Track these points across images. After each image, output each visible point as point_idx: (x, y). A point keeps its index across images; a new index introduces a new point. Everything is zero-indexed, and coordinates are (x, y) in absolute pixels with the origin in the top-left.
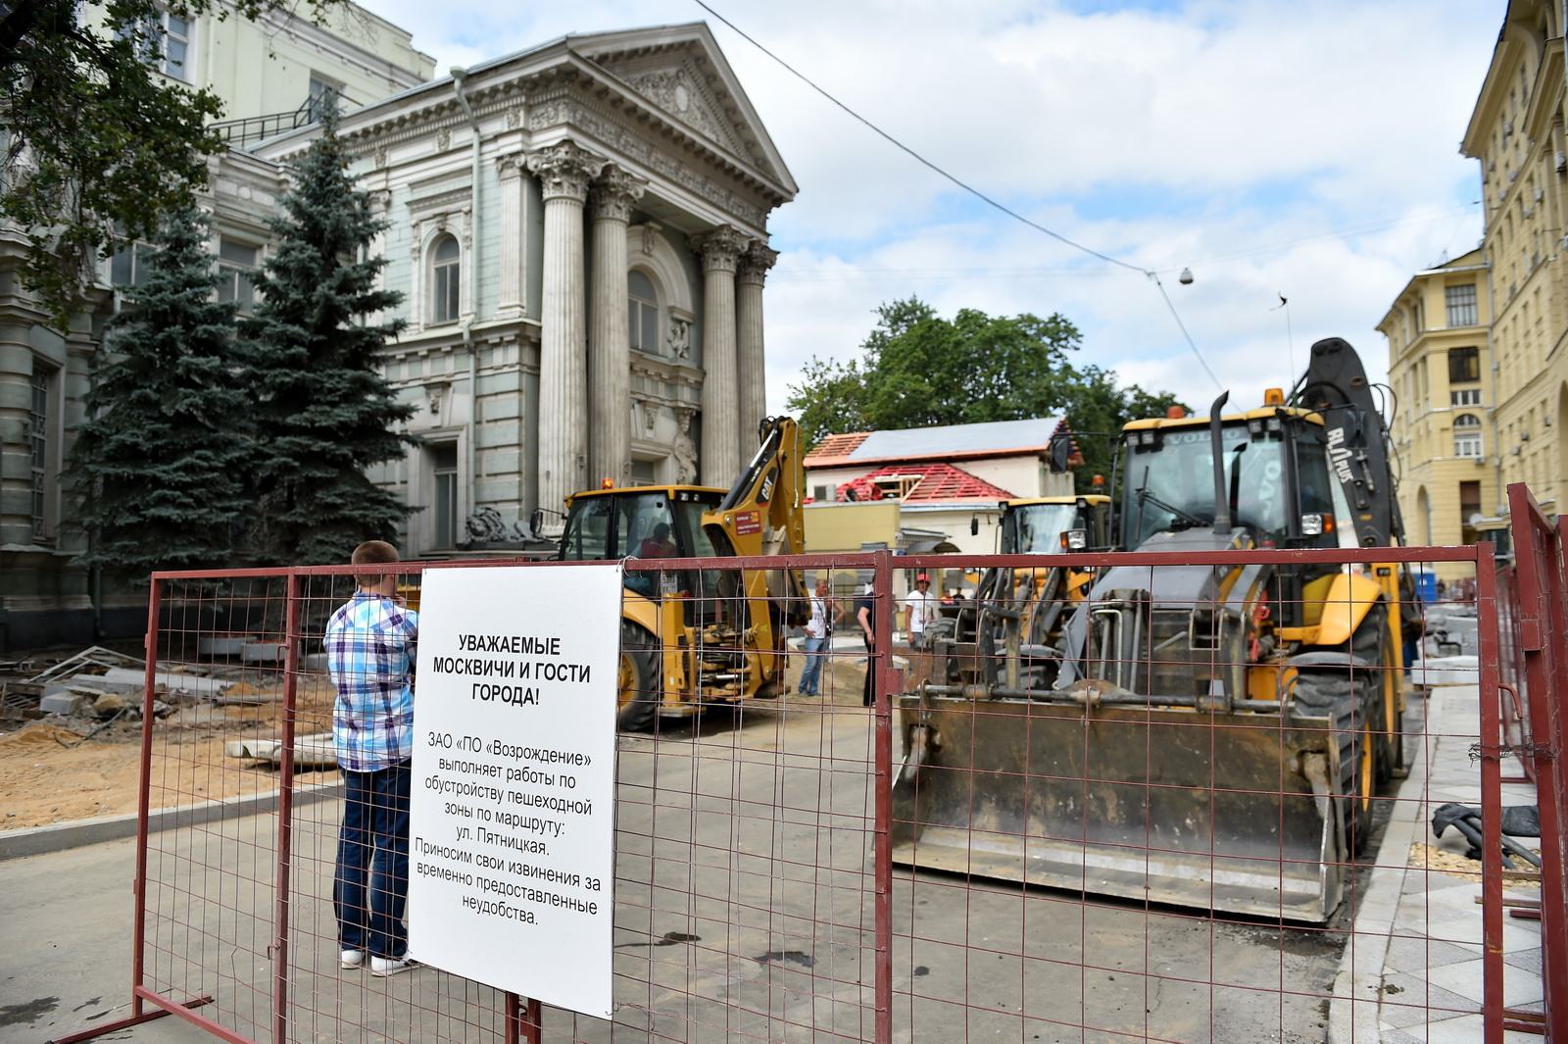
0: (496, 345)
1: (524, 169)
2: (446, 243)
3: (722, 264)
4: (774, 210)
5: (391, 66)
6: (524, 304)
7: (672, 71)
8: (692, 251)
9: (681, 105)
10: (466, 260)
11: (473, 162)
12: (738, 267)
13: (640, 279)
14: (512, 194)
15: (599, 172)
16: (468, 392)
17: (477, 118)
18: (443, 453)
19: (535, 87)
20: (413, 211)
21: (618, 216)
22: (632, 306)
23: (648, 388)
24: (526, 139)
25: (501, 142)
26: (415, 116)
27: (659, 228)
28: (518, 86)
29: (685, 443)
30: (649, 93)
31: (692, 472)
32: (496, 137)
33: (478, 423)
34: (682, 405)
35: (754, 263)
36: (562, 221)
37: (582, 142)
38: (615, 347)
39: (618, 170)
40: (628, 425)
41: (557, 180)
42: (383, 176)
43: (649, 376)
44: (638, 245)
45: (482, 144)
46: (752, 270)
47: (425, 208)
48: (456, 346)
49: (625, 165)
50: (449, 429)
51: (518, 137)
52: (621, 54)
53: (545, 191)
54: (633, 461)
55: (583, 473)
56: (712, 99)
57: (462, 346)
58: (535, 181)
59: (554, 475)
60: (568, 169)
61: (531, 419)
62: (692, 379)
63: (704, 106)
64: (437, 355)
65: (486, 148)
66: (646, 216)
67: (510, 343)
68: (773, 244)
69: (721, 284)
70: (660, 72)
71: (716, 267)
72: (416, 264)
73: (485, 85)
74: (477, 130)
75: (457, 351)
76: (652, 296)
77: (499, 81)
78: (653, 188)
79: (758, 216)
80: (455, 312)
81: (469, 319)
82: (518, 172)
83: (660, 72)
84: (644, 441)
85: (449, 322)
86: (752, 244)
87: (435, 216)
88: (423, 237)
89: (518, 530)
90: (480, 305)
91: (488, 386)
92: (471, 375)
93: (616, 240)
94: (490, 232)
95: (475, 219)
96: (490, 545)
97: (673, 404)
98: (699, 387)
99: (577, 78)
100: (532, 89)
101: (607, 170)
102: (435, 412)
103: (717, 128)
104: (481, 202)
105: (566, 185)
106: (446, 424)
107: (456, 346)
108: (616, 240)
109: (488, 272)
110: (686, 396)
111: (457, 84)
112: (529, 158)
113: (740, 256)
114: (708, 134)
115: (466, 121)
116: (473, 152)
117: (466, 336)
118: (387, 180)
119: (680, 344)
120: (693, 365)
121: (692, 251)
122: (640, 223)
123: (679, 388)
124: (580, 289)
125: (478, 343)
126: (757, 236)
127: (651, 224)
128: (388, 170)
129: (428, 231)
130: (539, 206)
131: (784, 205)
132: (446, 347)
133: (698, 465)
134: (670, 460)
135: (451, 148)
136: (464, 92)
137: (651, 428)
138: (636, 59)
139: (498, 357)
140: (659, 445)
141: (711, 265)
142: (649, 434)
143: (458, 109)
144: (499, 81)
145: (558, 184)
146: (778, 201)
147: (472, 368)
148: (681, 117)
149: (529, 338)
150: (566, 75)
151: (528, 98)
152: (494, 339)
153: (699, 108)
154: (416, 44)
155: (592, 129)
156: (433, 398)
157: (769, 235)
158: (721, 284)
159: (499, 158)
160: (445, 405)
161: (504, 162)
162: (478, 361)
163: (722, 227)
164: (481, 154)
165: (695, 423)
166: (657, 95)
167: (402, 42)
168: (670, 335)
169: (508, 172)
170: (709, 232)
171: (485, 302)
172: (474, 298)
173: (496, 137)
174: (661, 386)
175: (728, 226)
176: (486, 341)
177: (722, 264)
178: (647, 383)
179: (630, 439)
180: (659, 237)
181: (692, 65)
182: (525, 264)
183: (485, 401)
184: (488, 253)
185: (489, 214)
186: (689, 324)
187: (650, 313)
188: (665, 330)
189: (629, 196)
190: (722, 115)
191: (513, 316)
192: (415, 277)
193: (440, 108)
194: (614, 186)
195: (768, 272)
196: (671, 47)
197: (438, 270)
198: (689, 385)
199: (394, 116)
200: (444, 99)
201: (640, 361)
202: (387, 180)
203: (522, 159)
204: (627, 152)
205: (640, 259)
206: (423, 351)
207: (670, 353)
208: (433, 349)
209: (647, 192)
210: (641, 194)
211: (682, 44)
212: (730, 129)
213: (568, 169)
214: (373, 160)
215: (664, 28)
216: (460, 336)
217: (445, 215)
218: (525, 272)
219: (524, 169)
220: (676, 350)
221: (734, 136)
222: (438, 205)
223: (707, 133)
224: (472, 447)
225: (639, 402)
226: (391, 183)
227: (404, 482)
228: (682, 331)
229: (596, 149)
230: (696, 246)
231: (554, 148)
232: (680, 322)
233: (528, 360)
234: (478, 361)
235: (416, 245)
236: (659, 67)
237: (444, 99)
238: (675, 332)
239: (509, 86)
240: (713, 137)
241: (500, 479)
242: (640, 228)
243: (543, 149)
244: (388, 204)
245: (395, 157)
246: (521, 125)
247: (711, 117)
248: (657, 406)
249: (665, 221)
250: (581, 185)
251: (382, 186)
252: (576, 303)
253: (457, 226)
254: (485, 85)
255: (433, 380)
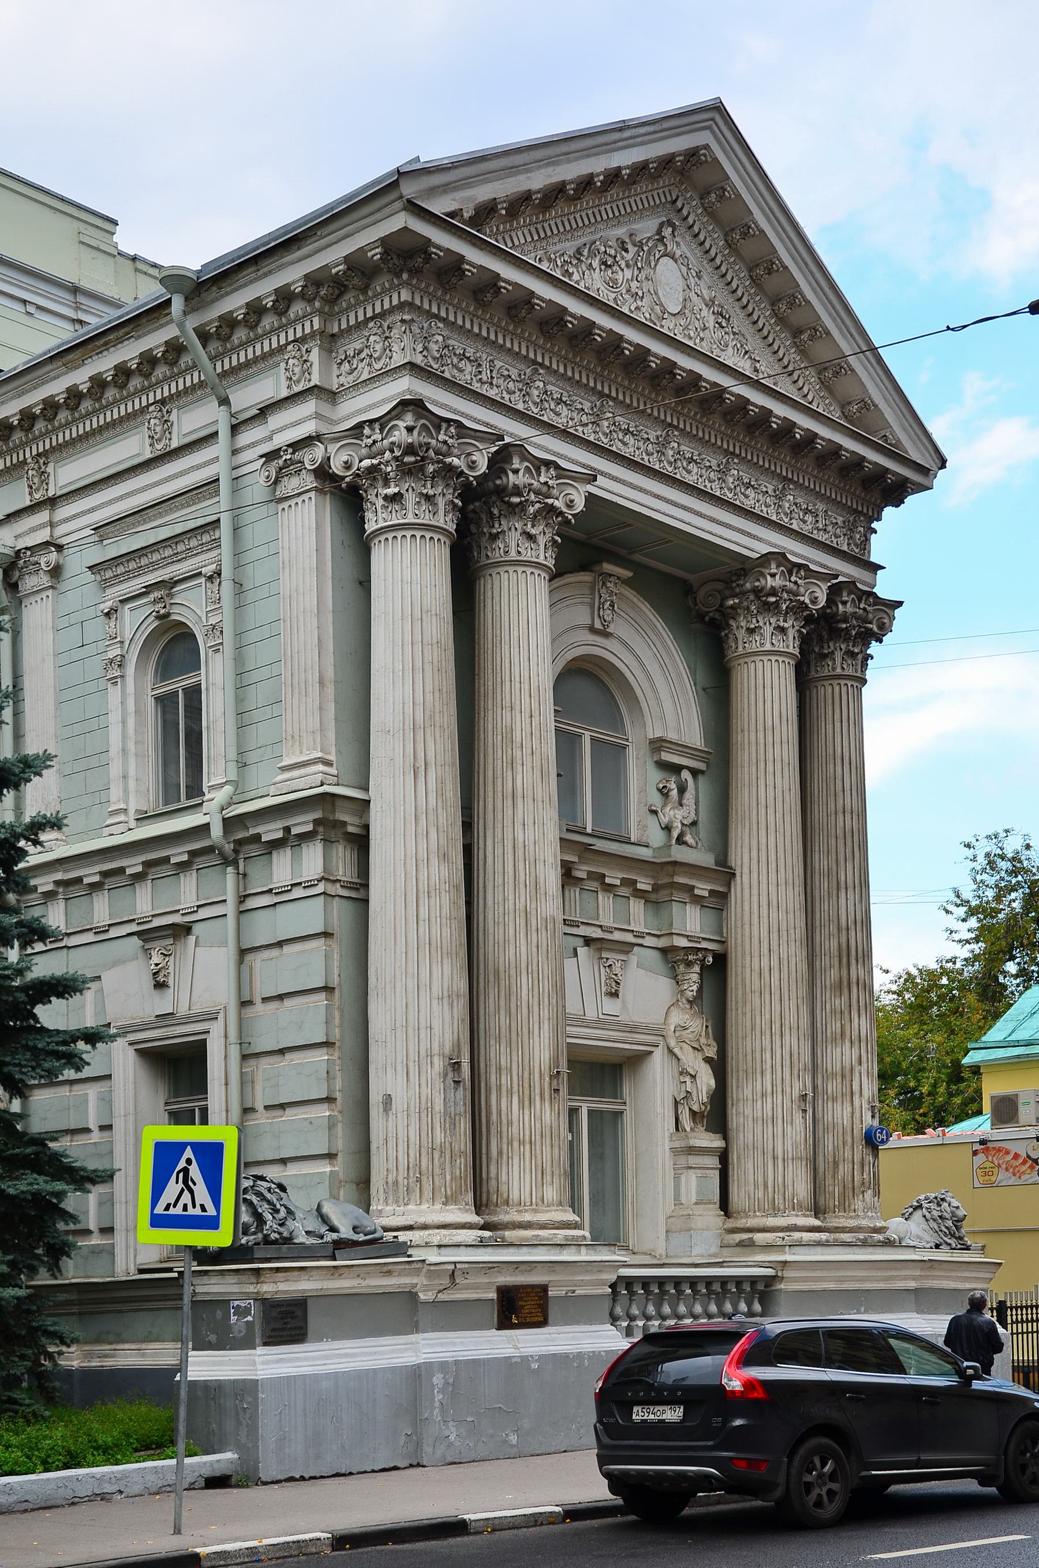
0: (276, 845)
1: (323, 473)
2: (174, 647)
3: (767, 639)
4: (888, 512)
5: (75, 290)
6: (332, 757)
7: (646, 227)
8: (701, 617)
9: (666, 294)
10: (215, 675)
11: (222, 469)
12: (805, 642)
13: (588, 685)
14: (304, 528)
15: (483, 467)
16: (225, 944)
17: (224, 374)
18: (180, 1067)
19: (331, 290)
20: (105, 585)
21: (528, 555)
22: (567, 744)
23: (606, 910)
24: (325, 409)
25: (275, 420)
26: (98, 384)
27: (627, 574)
28: (302, 296)
29: (697, 1026)
30: (595, 282)
31: (707, 1080)
32: (264, 412)
33: (245, 1004)
34: (683, 943)
35: (842, 630)
36: (411, 575)
37: (442, 401)
38: (529, 831)
39: (525, 456)
40: (560, 989)
41: (392, 490)
42: (43, 516)
43: (609, 888)
44: (582, 615)
45: (235, 429)
46: (838, 649)
47: (129, 575)
48: (198, 852)
49: (544, 446)
50: (189, 1020)
51: (309, 407)
52: (526, 197)
53: (369, 515)
54: (571, 1063)
55: (462, 1095)
56: (740, 278)
57: (210, 850)
58: (348, 496)
59: (398, 1104)
60: (413, 463)
61: (354, 991)
62: (703, 888)
63: (723, 298)
64: (164, 871)
65: (245, 438)
66: (596, 548)
67: (305, 837)
68: (884, 588)
69: (767, 684)
70: (621, 232)
71: (497, 556)
72: (114, 694)
73: (234, 302)
74: (224, 401)
75: (200, 862)
76: (616, 722)
77: (262, 288)
78: (606, 489)
79: (850, 528)
80: (195, 789)
81: (220, 796)
82: (310, 481)
83: (621, 232)
84: (599, 1024)
85: (185, 803)
86: (835, 591)
87: (149, 589)
88: (128, 636)
89: (324, 1219)
90: (242, 766)
91: (264, 928)
92: (230, 909)
93: (528, 616)
94: (258, 613)
95: (227, 587)
96: (270, 1251)
97: (662, 943)
98: (719, 902)
99: (413, 254)
100: (332, 301)
101: (500, 461)
102: (160, 986)
103: (754, 343)
104: (237, 554)
105: (410, 499)
106: (183, 1010)
107: (198, 852)
108: (528, 616)
109: (257, 696)
110: (691, 922)
111: (178, 304)
112: (332, 448)
113: (809, 620)
114: (734, 355)
115: (202, 384)
116: (219, 449)
117: (217, 831)
118: (52, 525)
119: (676, 816)
120: (705, 858)
121: (701, 617)
122: (584, 567)
123: (676, 907)
124: (448, 717)
125: (242, 842)
126: (847, 570)
127: (608, 567)
128: (52, 502)
129: (136, 622)
130: (360, 546)
131: (909, 500)
132: (178, 854)
133: (720, 1067)
134: (658, 1056)
135: (175, 444)
136: (192, 323)
137: (615, 995)
138: (561, 207)
139: (282, 869)
140: (633, 1029)
141: (741, 642)
142: (610, 1006)
143: (185, 360)
144: (262, 288)
145: (395, 499)
146: (896, 492)
147: (231, 897)
148: (667, 327)
149: (340, 823)
150: (405, 256)
151: (327, 317)
152: (271, 831)
153: (710, 303)
154: (126, 241)
155: (466, 375)
156: (156, 958)
157: (876, 568)
158: (767, 684)
159: (270, 456)
160: (178, 971)
161: (281, 461)
162: (243, 876)
163: (765, 559)
164: (235, 452)
165: (714, 973)
166: (612, 284)
167: (93, 237)
168: (656, 800)
169: (291, 485)
170: (743, 568)
171: (252, 757)
172: (232, 754)
173: (264, 412)
174: (637, 907)
175: (780, 557)
176: (257, 838)
177: (767, 639)
178: (605, 901)
179: (563, 1019)
180: (629, 593)
181: (694, 213)
182: (330, 673)
183: (257, 960)
184: (258, 655)
185: (257, 574)
186: (695, 773)
187: (611, 754)
188: (643, 790)
189: (551, 510)
190: (764, 314)
191: (309, 782)
192: (114, 718)
193: (148, 361)
194: (517, 491)
195: (874, 648)
196: (641, 169)
197: (159, 699)
198: (697, 900)
199: (57, 388)
200: (155, 340)
201: (584, 862)
202: (52, 525)
203: (318, 452)
204: (617, 447)
205: (585, 644)
206: (133, 865)
207: (656, 837)
208: (153, 859)
209: (591, 499)
210: (580, 505)
211: (667, 162)
212: (784, 342)
213: (413, 463)
214: (23, 485)
215: (622, 127)
216: (204, 829)
217: (170, 585)
218: (330, 690)
219: (323, 473)
220: (668, 829)
221: (793, 355)
222: (154, 566)
223: (730, 358)
224: (235, 1053)
225: (588, 941)
226: (60, 531)
227: (106, 1128)
228: (682, 790)
229: (477, 415)
230: (702, 599)
231: (382, 422)
232: (676, 769)
233: (344, 867)
234: (243, 876)
235: (114, 652)
236: (617, 220)
237: (155, 340)
238: (664, 792)
239: (285, 297)
240: (744, 366)
241: (291, 1114)
242: (586, 577)
243: (360, 426)
244: (56, 572)
245: (67, 474)
246: (315, 380)
247: (739, 321)
248: (626, 948)
249: (637, 557)
250: (445, 496)
251: (43, 536)
252: (442, 748)
253: (193, 607)
254: (234, 302)
255: (157, 922)
